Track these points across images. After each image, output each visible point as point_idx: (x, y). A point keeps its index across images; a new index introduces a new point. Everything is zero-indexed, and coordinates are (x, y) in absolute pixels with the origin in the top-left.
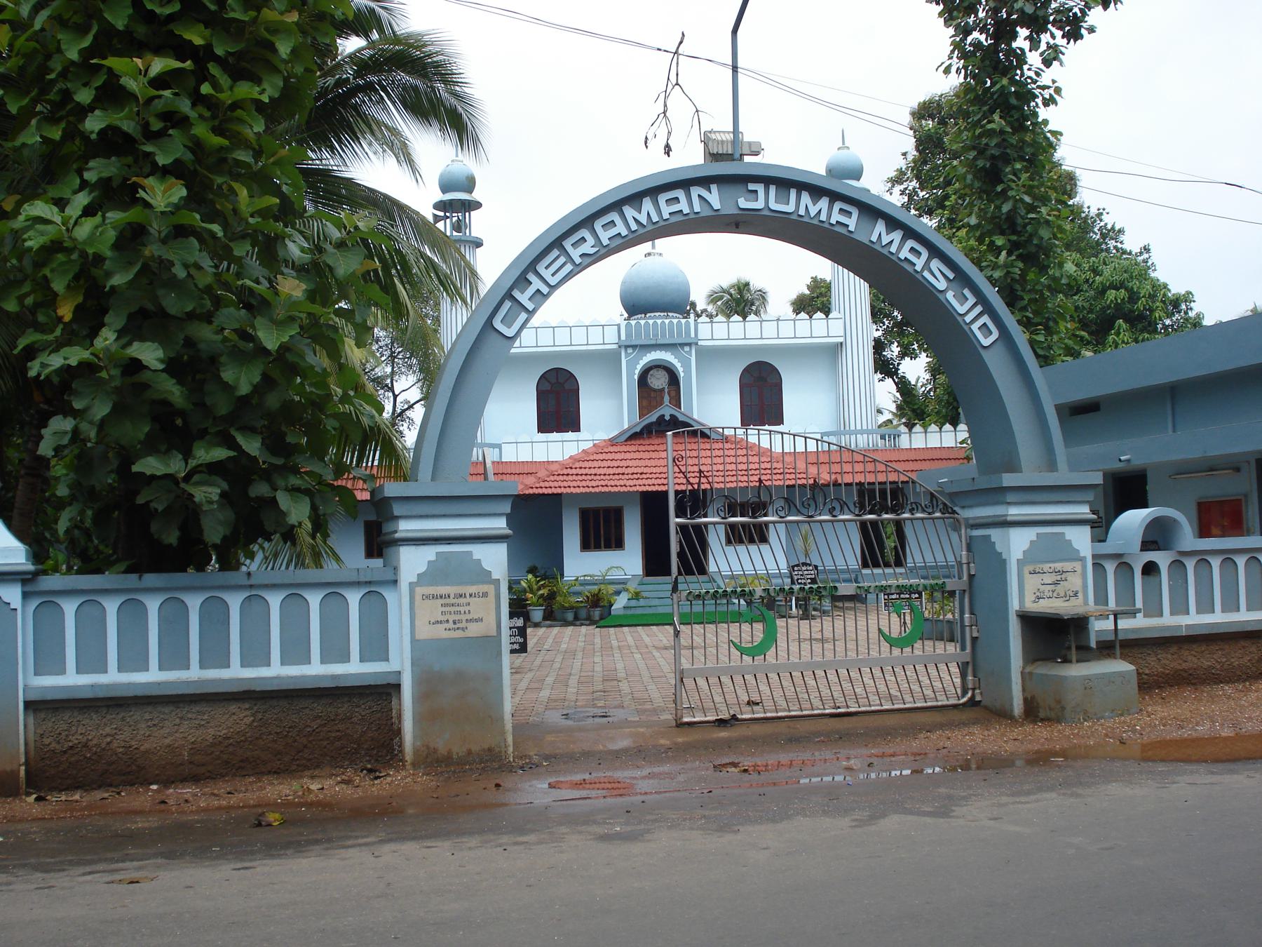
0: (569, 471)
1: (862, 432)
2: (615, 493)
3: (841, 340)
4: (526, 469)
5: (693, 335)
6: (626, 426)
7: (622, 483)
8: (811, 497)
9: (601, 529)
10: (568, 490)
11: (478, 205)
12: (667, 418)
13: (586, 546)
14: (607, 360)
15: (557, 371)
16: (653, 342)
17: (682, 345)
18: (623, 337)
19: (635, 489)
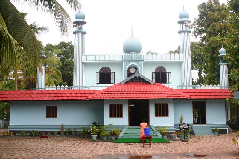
0: (106, 92)
1: (188, 86)
2: (120, 99)
3: (183, 61)
4: (93, 92)
5: (143, 58)
6: (124, 80)
7: (123, 96)
8: (180, 101)
9: (116, 112)
10: (106, 98)
11: (85, 23)
12: (137, 77)
13: (111, 116)
14: (119, 65)
15: (105, 67)
16: (132, 60)
18: (123, 58)
19: (127, 98)
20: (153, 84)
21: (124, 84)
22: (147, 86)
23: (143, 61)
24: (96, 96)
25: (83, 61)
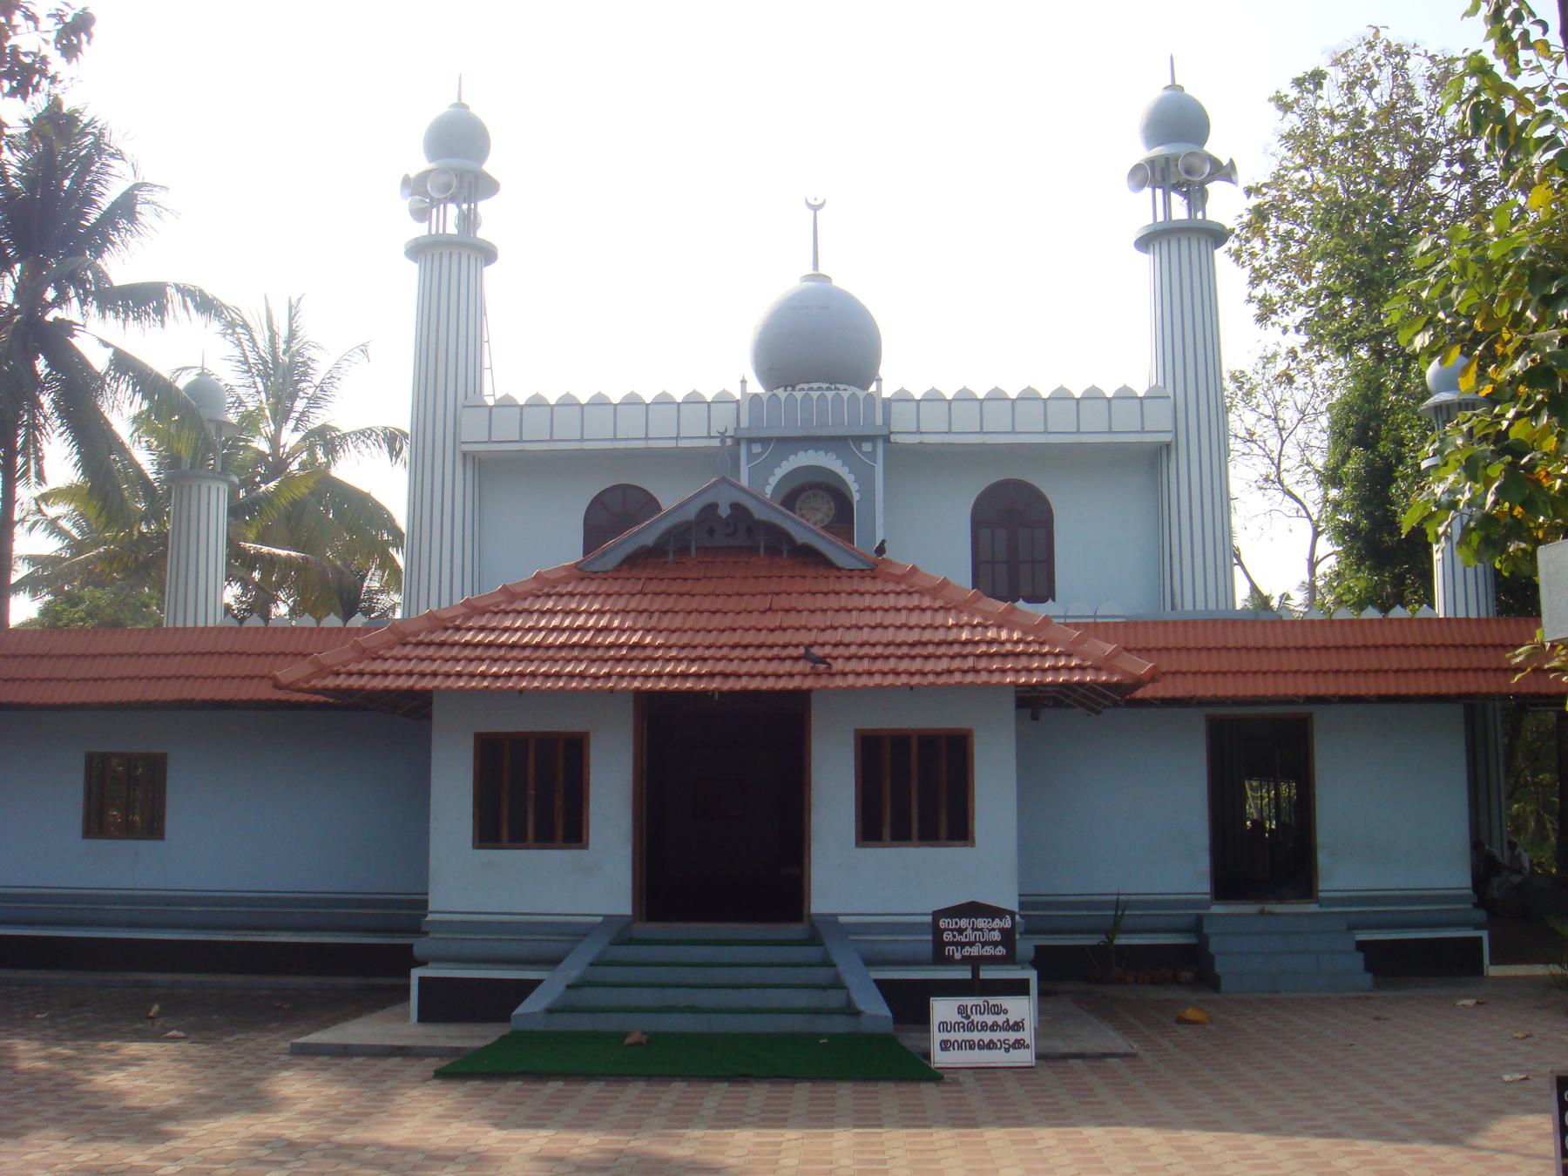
3: (1167, 438)
5: (879, 420)
9: (530, 792)
12: (724, 511)
13: (489, 833)
15: (623, 490)
17: (860, 439)
20: (851, 573)
21: (618, 568)
22: (799, 585)
23: (886, 439)
24: (353, 667)
25: (466, 448)
